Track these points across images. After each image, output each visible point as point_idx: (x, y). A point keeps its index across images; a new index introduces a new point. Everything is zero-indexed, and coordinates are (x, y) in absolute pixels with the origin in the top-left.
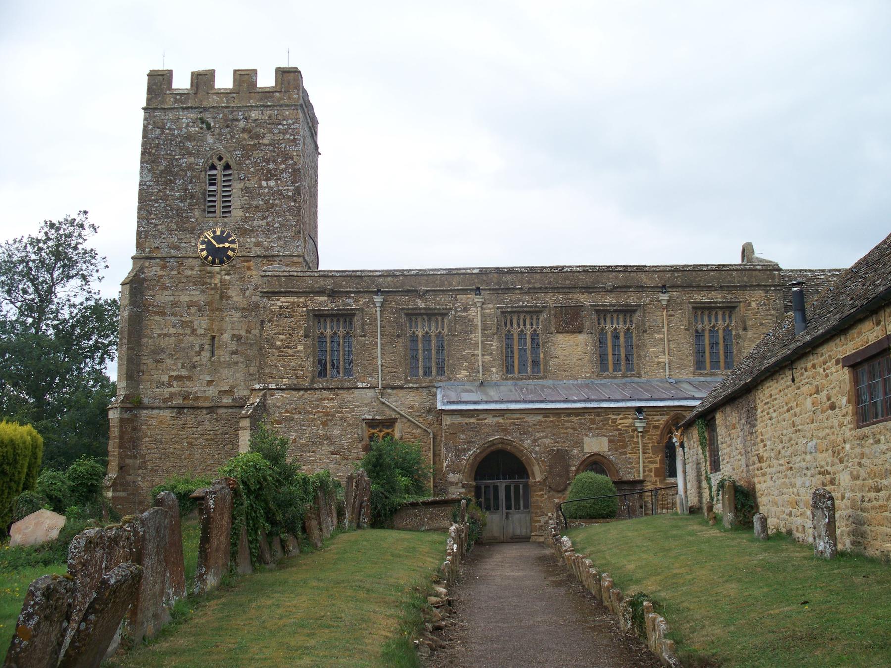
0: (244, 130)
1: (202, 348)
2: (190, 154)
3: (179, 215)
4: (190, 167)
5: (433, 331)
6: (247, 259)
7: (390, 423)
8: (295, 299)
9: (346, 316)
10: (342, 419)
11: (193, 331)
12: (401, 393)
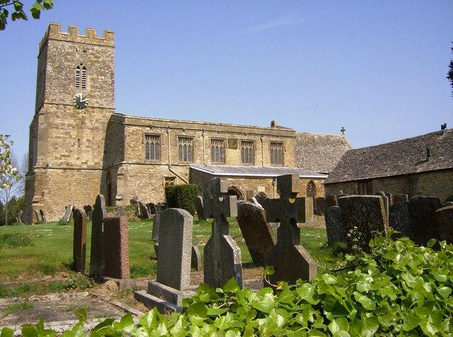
0: (91, 54)
1: (74, 144)
2: (69, 61)
3: (64, 86)
4: (69, 66)
5: (249, 147)
6: (93, 108)
7: (173, 179)
8: (138, 128)
9: (157, 136)
10: (156, 176)
11: (71, 136)
12: (177, 167)
